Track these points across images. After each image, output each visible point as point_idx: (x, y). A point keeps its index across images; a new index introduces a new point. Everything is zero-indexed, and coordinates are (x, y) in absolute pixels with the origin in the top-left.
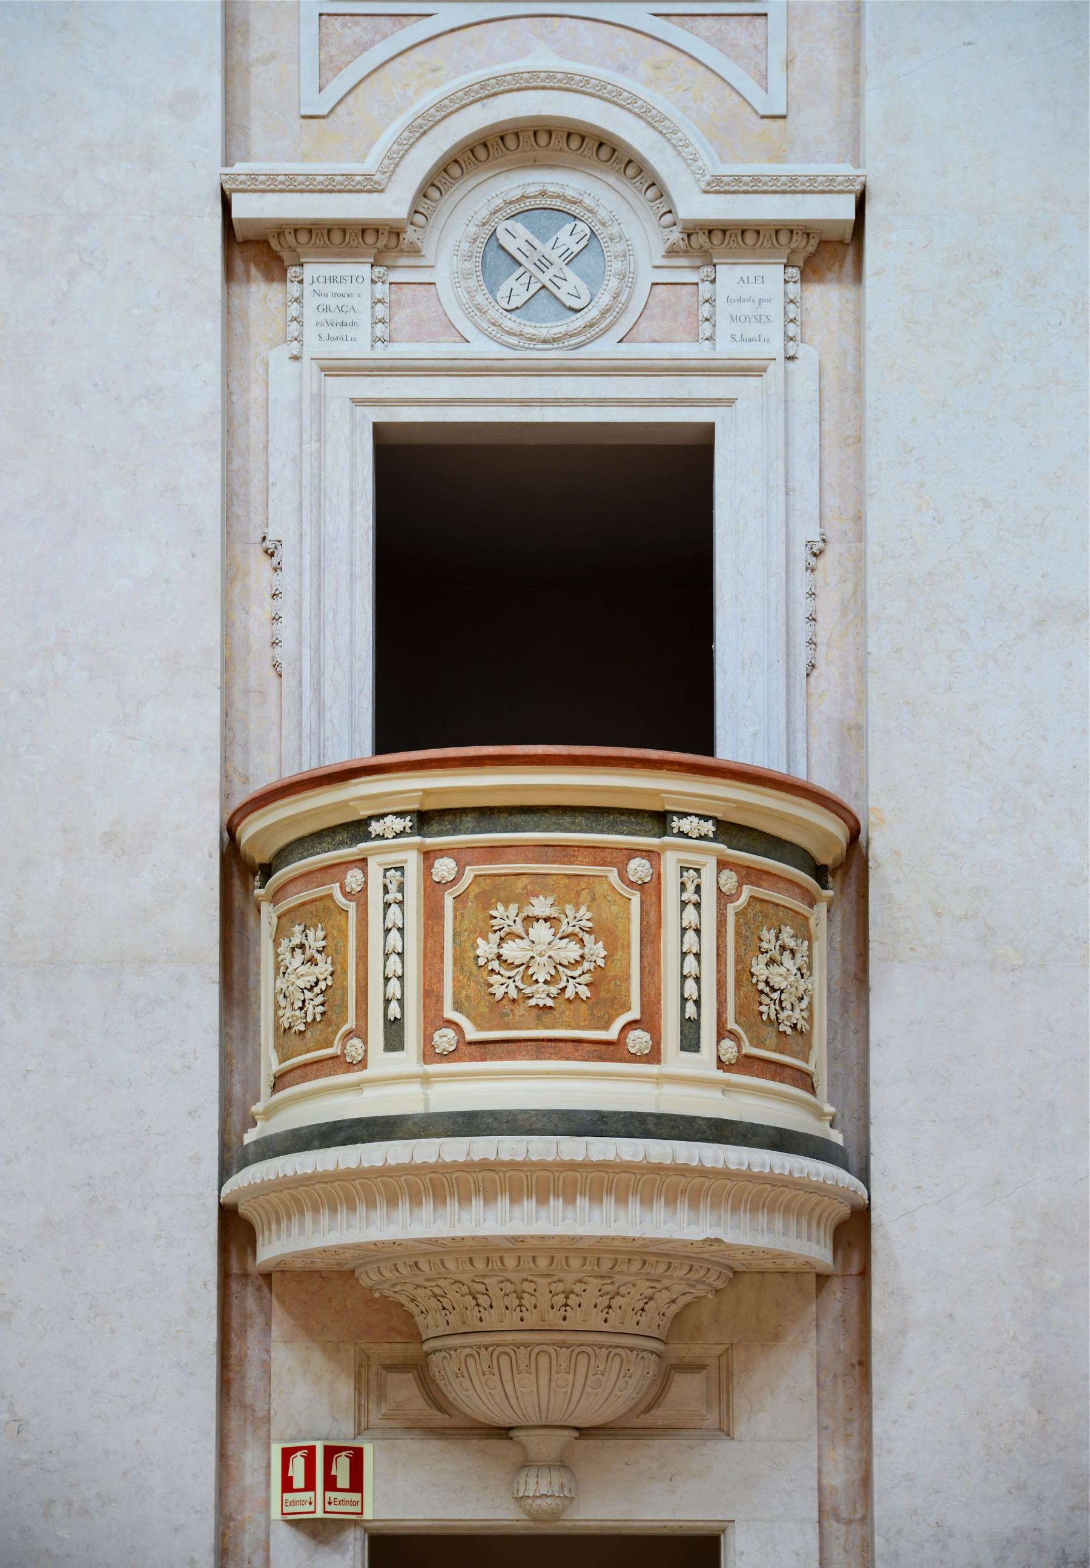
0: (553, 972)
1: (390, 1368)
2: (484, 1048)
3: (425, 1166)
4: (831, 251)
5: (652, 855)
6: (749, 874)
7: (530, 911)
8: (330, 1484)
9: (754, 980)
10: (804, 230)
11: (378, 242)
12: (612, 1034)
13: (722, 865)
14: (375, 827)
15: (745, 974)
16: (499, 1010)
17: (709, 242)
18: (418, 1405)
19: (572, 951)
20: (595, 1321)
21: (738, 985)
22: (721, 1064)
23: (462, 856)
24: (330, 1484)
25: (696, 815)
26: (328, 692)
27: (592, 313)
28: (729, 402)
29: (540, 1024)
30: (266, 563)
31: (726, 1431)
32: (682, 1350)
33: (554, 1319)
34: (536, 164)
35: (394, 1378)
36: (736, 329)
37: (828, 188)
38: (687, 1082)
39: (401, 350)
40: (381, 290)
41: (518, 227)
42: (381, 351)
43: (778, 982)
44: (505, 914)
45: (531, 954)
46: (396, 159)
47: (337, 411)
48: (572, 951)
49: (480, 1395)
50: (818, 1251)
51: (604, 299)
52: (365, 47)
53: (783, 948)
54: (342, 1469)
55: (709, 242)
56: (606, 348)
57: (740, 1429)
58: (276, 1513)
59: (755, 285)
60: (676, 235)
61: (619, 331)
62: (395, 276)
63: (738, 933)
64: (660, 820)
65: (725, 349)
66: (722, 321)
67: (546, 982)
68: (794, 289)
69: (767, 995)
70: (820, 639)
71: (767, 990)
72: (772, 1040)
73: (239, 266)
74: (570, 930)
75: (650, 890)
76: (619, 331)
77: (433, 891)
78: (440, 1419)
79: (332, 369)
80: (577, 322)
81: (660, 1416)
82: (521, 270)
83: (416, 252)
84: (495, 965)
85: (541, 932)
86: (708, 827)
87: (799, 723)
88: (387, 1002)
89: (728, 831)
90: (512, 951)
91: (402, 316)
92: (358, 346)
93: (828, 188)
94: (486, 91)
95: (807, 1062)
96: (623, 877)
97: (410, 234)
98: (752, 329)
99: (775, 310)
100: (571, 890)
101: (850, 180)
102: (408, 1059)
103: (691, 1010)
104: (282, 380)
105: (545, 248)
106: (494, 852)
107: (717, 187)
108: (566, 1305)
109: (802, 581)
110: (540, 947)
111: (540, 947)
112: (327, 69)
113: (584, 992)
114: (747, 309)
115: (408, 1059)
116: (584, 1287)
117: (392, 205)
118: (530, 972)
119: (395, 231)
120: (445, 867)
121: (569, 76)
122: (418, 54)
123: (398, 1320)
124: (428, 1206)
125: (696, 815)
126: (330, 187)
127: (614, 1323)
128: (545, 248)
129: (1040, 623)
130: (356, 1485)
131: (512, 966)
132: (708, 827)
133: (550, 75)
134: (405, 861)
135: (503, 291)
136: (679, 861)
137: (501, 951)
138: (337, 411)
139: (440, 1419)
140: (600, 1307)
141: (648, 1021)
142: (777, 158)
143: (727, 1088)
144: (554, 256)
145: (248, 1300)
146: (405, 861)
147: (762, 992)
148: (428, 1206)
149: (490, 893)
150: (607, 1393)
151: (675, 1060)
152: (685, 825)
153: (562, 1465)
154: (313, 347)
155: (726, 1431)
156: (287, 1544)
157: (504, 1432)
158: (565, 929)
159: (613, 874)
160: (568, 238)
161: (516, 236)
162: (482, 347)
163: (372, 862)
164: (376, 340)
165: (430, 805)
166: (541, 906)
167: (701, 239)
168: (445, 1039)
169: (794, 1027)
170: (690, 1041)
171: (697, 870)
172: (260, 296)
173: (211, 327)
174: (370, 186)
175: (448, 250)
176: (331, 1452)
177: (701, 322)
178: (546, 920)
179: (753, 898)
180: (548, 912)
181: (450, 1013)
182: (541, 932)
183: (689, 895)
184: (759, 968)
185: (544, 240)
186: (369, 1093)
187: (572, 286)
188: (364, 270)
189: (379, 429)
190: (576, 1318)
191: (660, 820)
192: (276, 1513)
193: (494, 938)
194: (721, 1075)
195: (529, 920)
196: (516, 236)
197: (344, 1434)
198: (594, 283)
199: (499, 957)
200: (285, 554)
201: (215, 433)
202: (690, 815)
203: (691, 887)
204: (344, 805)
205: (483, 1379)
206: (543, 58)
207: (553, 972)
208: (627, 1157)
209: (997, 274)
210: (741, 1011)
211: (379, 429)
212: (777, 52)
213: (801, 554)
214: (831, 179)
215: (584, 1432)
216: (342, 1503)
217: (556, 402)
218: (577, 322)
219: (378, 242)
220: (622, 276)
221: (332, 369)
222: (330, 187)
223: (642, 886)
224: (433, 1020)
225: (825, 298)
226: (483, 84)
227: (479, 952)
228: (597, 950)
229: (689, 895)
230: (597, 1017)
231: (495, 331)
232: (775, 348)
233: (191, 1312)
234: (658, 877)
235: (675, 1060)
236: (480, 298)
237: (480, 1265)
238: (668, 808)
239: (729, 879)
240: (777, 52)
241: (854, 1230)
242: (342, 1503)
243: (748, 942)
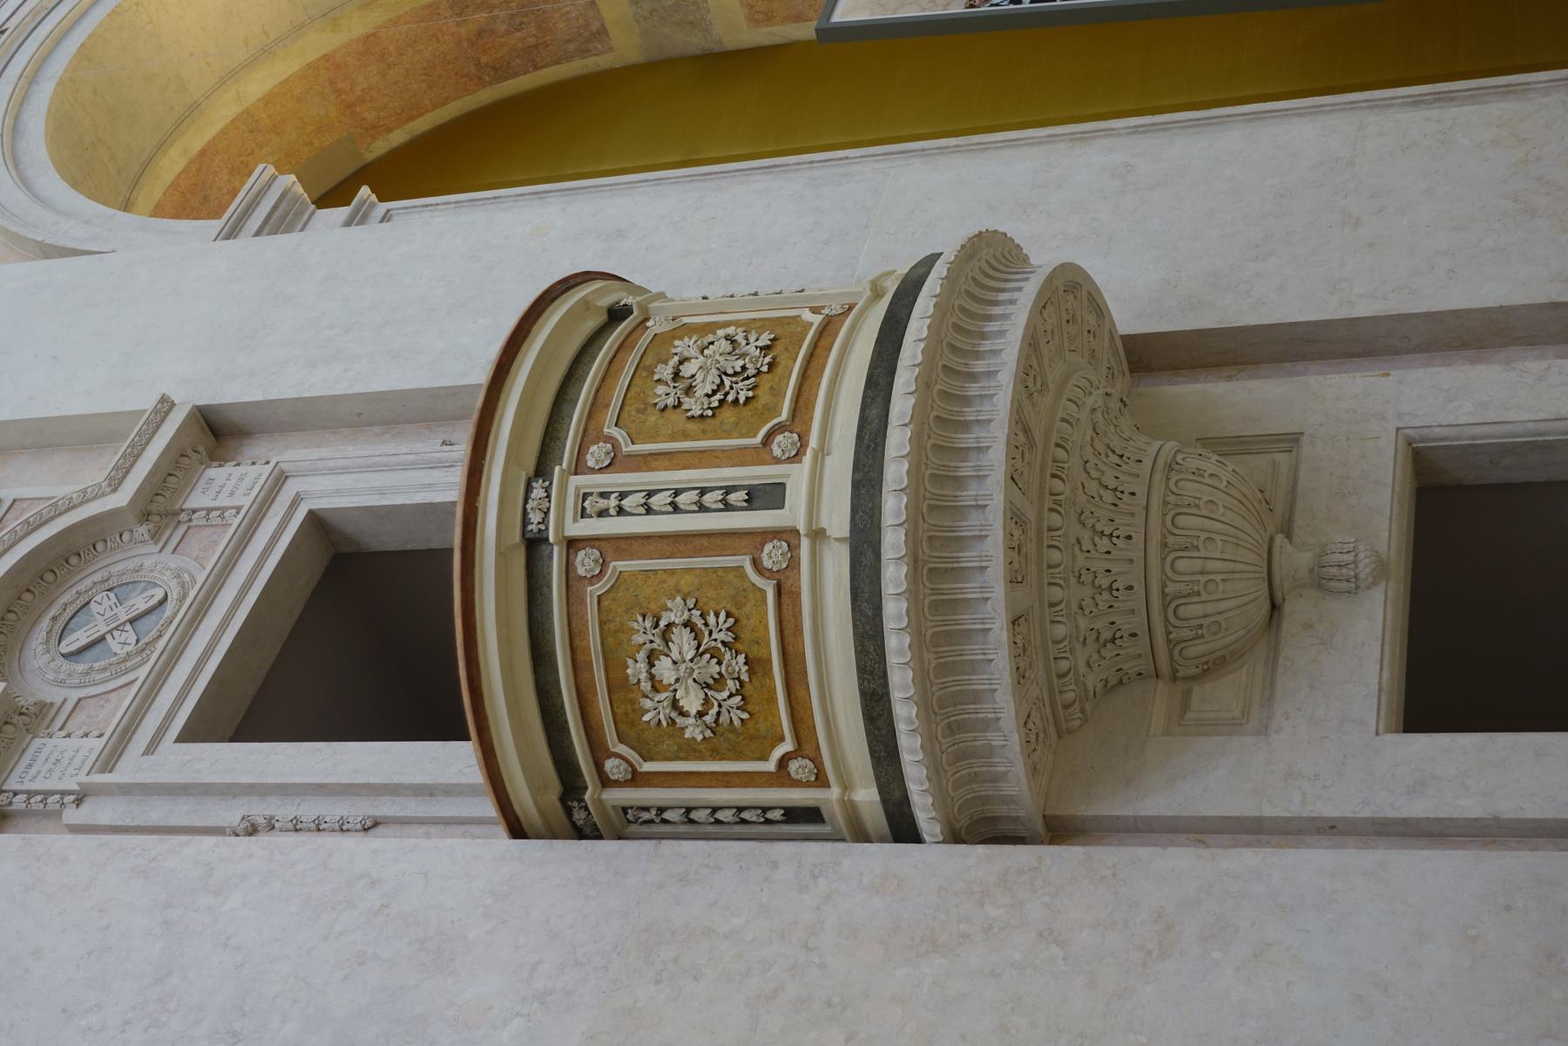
0: (708, 656)
5: (572, 544)
7: (646, 686)
9: (710, 413)
13: (579, 468)
25: (526, 501)
29: (768, 673)
44: (654, 710)
45: (690, 681)
64: (534, 545)
67: (719, 663)
69: (726, 394)
71: (719, 396)
74: (658, 640)
82: (108, 637)
84: (709, 719)
85: (665, 670)
88: (768, 822)
90: (692, 701)
95: (812, 324)
108: (1110, 588)
115: (797, 479)
116: (1083, 572)
118: (711, 682)
125: (526, 501)
131: (707, 700)
134: (788, 476)
136: (575, 520)
137: (693, 712)
140: (1109, 547)
143: (822, 452)
146: (788, 476)
147: (721, 402)
152: (535, 517)
158: (658, 643)
159: (787, 746)
166: (637, 669)
169: (766, 349)
171: (585, 496)
178: (652, 665)
180: (643, 666)
182: (665, 670)
184: (694, 406)
191: (534, 545)
193: (680, 721)
194: (808, 458)
195: (656, 687)
199: (700, 714)
202: (525, 510)
203: (603, 503)
205: (1204, 597)
207: (708, 656)
227: (700, 738)
235: (793, 513)
238: (517, 537)
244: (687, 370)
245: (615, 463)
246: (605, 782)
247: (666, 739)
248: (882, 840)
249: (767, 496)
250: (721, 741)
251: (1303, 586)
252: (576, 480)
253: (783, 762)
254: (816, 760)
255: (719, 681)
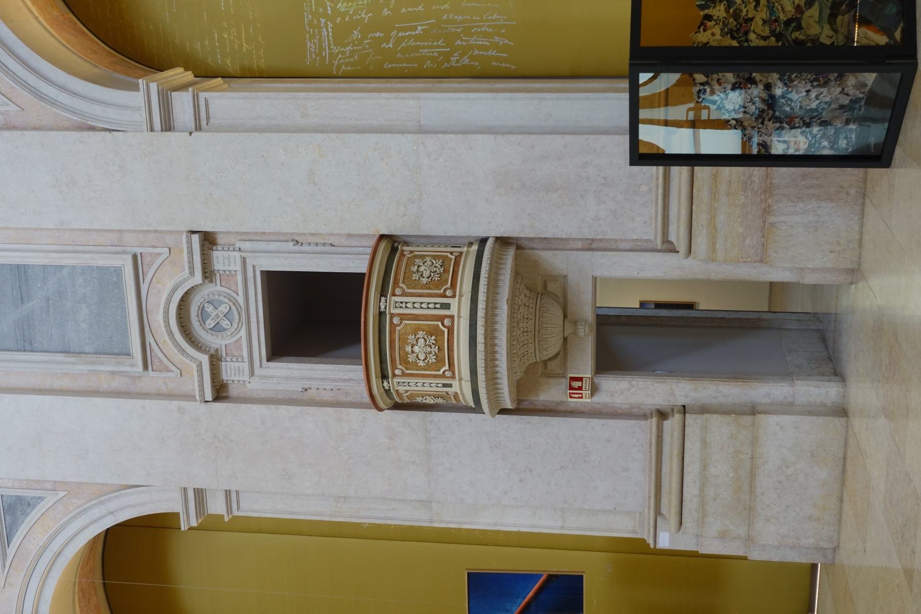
1: (546, 368)
2: (451, 364)
3: (485, 356)
4: (208, 240)
5: (392, 316)
6: (396, 284)
8: (580, 388)
10: (202, 246)
11: (215, 361)
12: (446, 330)
13: (394, 295)
14: (382, 310)
15: (426, 286)
16: (440, 361)
17: (208, 273)
18: (557, 362)
19: (421, 341)
20: (531, 322)
21: (429, 289)
22: (454, 296)
23: (394, 367)
24: (580, 388)
26: (345, 377)
27: (231, 304)
28: (254, 266)
30: (309, 391)
31: (565, 276)
32: (540, 289)
33: (531, 335)
34: (189, 317)
35: (549, 367)
36: (232, 265)
37: (190, 243)
38: (459, 307)
39: (245, 353)
40: (228, 359)
41: (208, 322)
42: (246, 360)
43: (428, 273)
44: (411, 358)
46: (192, 358)
47: (264, 372)
48: (421, 341)
49: (553, 346)
50: (511, 253)
51: (226, 300)
52: (160, 361)
53: (418, 271)
54: (576, 384)
55: (208, 273)
56: (241, 299)
57: (564, 273)
58: (589, 400)
59: (221, 260)
60: (206, 281)
61: (235, 296)
62: (224, 355)
63: (414, 288)
64: (381, 315)
65: (238, 268)
66: (230, 268)
68: (219, 248)
70: (322, 241)
72: (445, 275)
73: (224, 394)
75: (403, 317)
76: (235, 296)
77: (404, 375)
78: (561, 354)
79: (252, 373)
80: (233, 308)
81: (560, 294)
83: (217, 350)
85: (416, 349)
86: (383, 299)
87: (348, 250)
89: (383, 293)
90: (422, 357)
91: (235, 353)
92: (246, 366)
93: (190, 243)
94: (171, 334)
96: (399, 325)
97: (212, 352)
98: (232, 260)
99: (226, 254)
100: (403, 341)
101: (187, 237)
102: (454, 302)
103: (438, 306)
104: (255, 386)
105: (213, 315)
106: (393, 360)
107: (192, 273)
109: (305, 248)
110: (420, 350)
111: (420, 350)
112: (167, 370)
113: (433, 337)
114: (226, 262)
115: (454, 302)
117: (205, 359)
119: (211, 356)
120: (397, 372)
121: (164, 312)
122: (161, 346)
123: (530, 369)
124: (497, 363)
126: (201, 376)
127: (531, 341)
128: (213, 315)
129: (315, 184)
130: (580, 379)
132: (383, 299)
133: (164, 317)
135: (226, 327)
138: (264, 372)
139: (561, 354)
141: (441, 319)
142: (182, 250)
143: (461, 296)
144: (215, 313)
145: (525, 405)
148: (497, 363)
149: (405, 361)
150: (554, 313)
151: (453, 311)
152: (383, 307)
153: (575, 323)
154: (246, 377)
155: (565, 276)
156: (598, 398)
157: (565, 340)
159: (398, 328)
160: (209, 309)
161: (210, 323)
162: (243, 333)
163: (393, 311)
164: (243, 361)
165: (380, 375)
166: (408, 349)
167: (207, 275)
168: (449, 293)
170: (447, 306)
172: (233, 391)
173: (244, 407)
174: (200, 365)
175: (215, 342)
176: (571, 388)
177: (232, 274)
179: (403, 282)
181: (441, 372)
182: (416, 349)
183: (404, 305)
184: (424, 280)
185: (210, 316)
186: (465, 392)
187: (224, 309)
188: (223, 364)
189: (269, 360)
190: (531, 328)
191: (381, 315)
192: (589, 400)
195: (413, 352)
196: (210, 323)
197: (565, 382)
198: (222, 303)
200: (306, 387)
201: (273, 407)
204: (381, 396)
206: (160, 317)
208: (483, 332)
209: (211, 194)
210: (438, 288)
211: (269, 360)
212: (151, 250)
213: (298, 248)
214: (187, 242)
215: (565, 317)
216: (586, 385)
217: (257, 314)
218: (233, 308)
219: (215, 361)
220: (219, 295)
221: (252, 373)
222: (201, 376)
223: (401, 320)
224: (443, 376)
225: (221, 240)
226: (169, 335)
228: (421, 334)
229: (404, 305)
230: (439, 332)
231: (238, 330)
232: (237, 254)
233: (529, 423)
234: (399, 315)
235: (453, 311)
236: (229, 333)
237: (515, 343)
239: (398, 291)
240: (151, 250)
241: (503, 242)
242: (586, 385)
243: (415, 284)
244: (422, 269)
245: (404, 294)
246: (394, 375)
247: (415, 365)
248: (222, 232)
249: (447, 306)
250: (428, 367)
251: (518, 404)
252: (394, 298)
253: (444, 372)
254: (454, 373)
255: (430, 353)
